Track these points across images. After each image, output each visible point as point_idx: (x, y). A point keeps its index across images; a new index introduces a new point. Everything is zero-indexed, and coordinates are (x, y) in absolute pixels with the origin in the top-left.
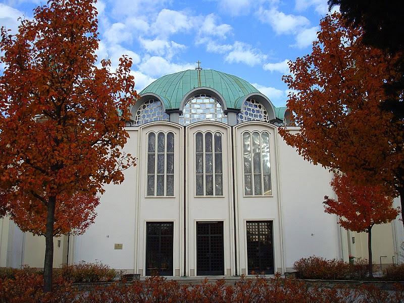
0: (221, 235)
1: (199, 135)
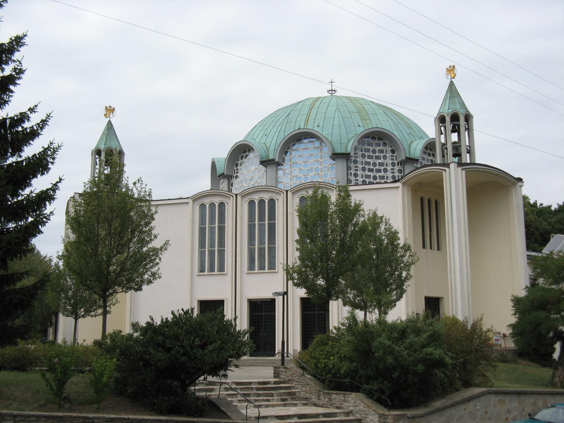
0: (305, 313)
1: (252, 203)
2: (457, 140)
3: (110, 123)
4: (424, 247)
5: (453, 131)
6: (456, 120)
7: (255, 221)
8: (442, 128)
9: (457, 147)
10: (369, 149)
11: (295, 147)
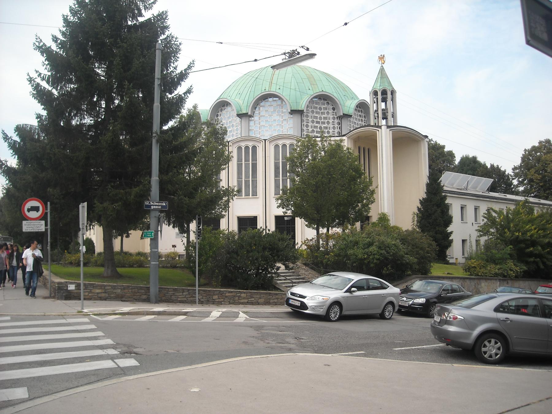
11: (262, 104)
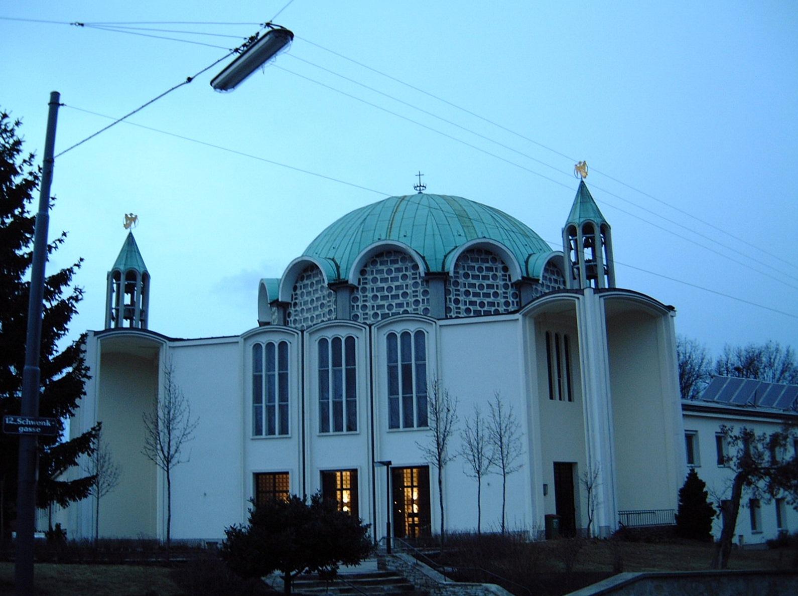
2: (591, 258)
3: (131, 238)
4: (551, 398)
5: (586, 245)
6: (589, 230)
7: (328, 366)
8: (572, 242)
9: (592, 271)
10: (474, 267)
